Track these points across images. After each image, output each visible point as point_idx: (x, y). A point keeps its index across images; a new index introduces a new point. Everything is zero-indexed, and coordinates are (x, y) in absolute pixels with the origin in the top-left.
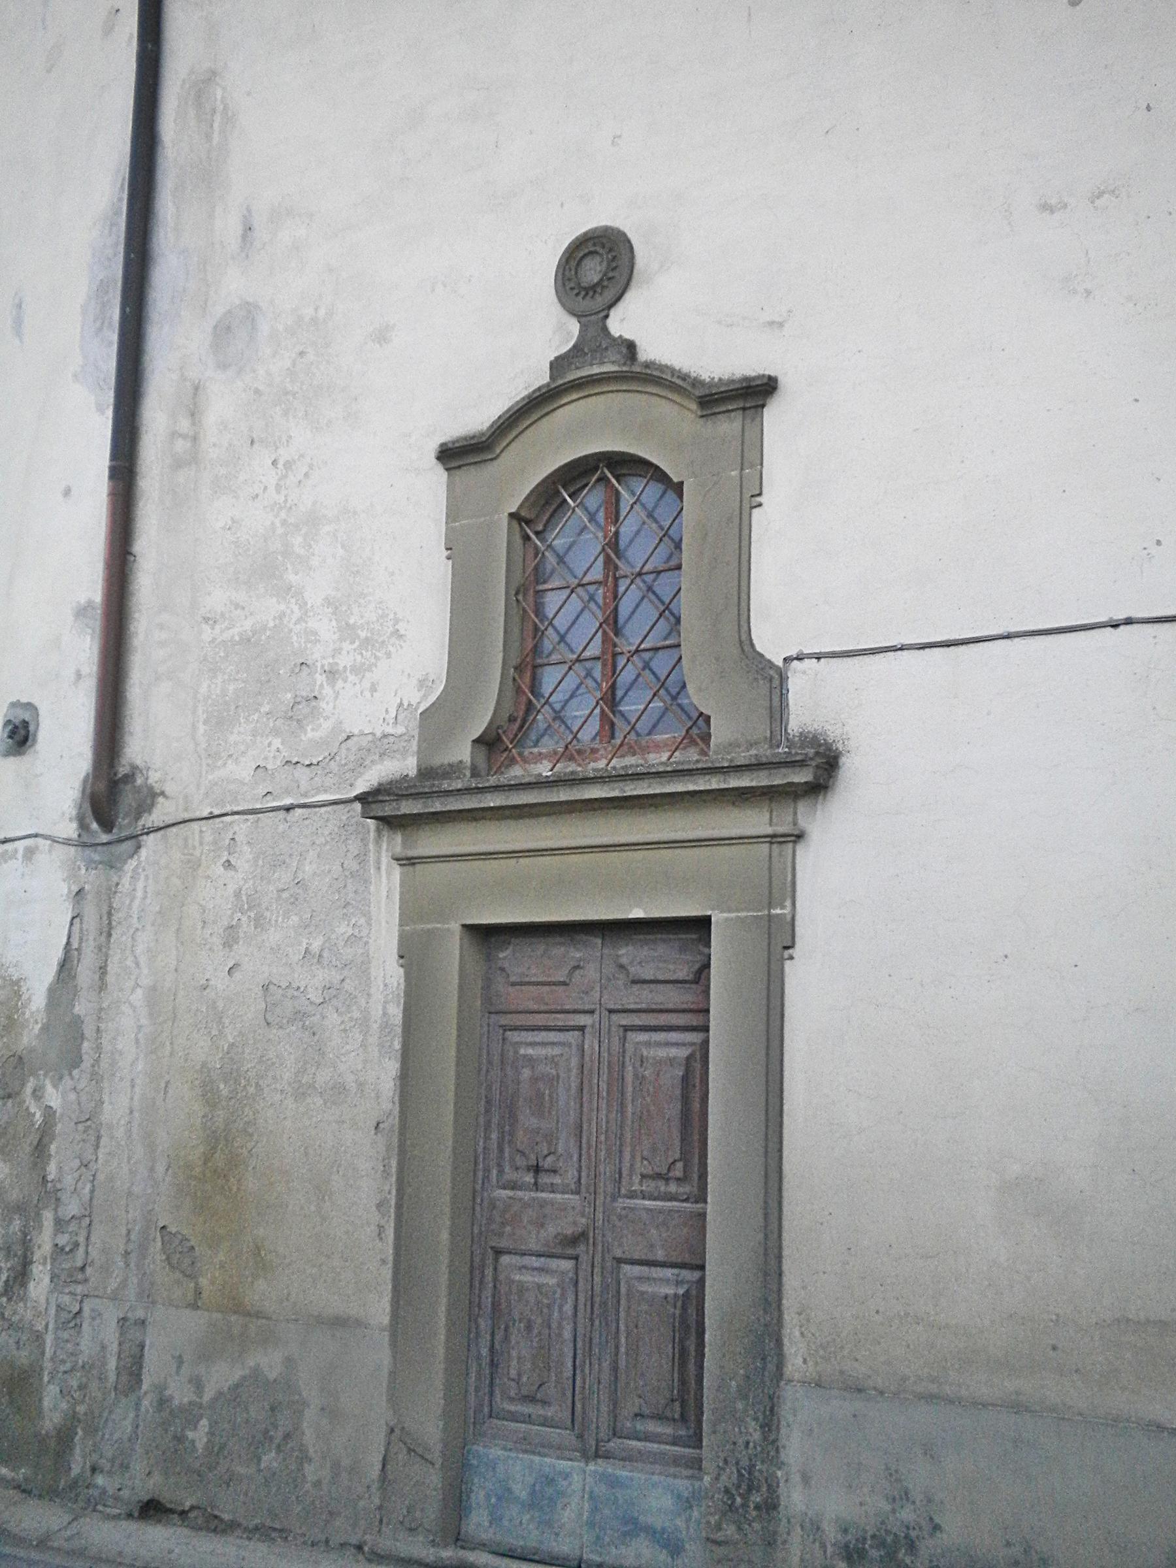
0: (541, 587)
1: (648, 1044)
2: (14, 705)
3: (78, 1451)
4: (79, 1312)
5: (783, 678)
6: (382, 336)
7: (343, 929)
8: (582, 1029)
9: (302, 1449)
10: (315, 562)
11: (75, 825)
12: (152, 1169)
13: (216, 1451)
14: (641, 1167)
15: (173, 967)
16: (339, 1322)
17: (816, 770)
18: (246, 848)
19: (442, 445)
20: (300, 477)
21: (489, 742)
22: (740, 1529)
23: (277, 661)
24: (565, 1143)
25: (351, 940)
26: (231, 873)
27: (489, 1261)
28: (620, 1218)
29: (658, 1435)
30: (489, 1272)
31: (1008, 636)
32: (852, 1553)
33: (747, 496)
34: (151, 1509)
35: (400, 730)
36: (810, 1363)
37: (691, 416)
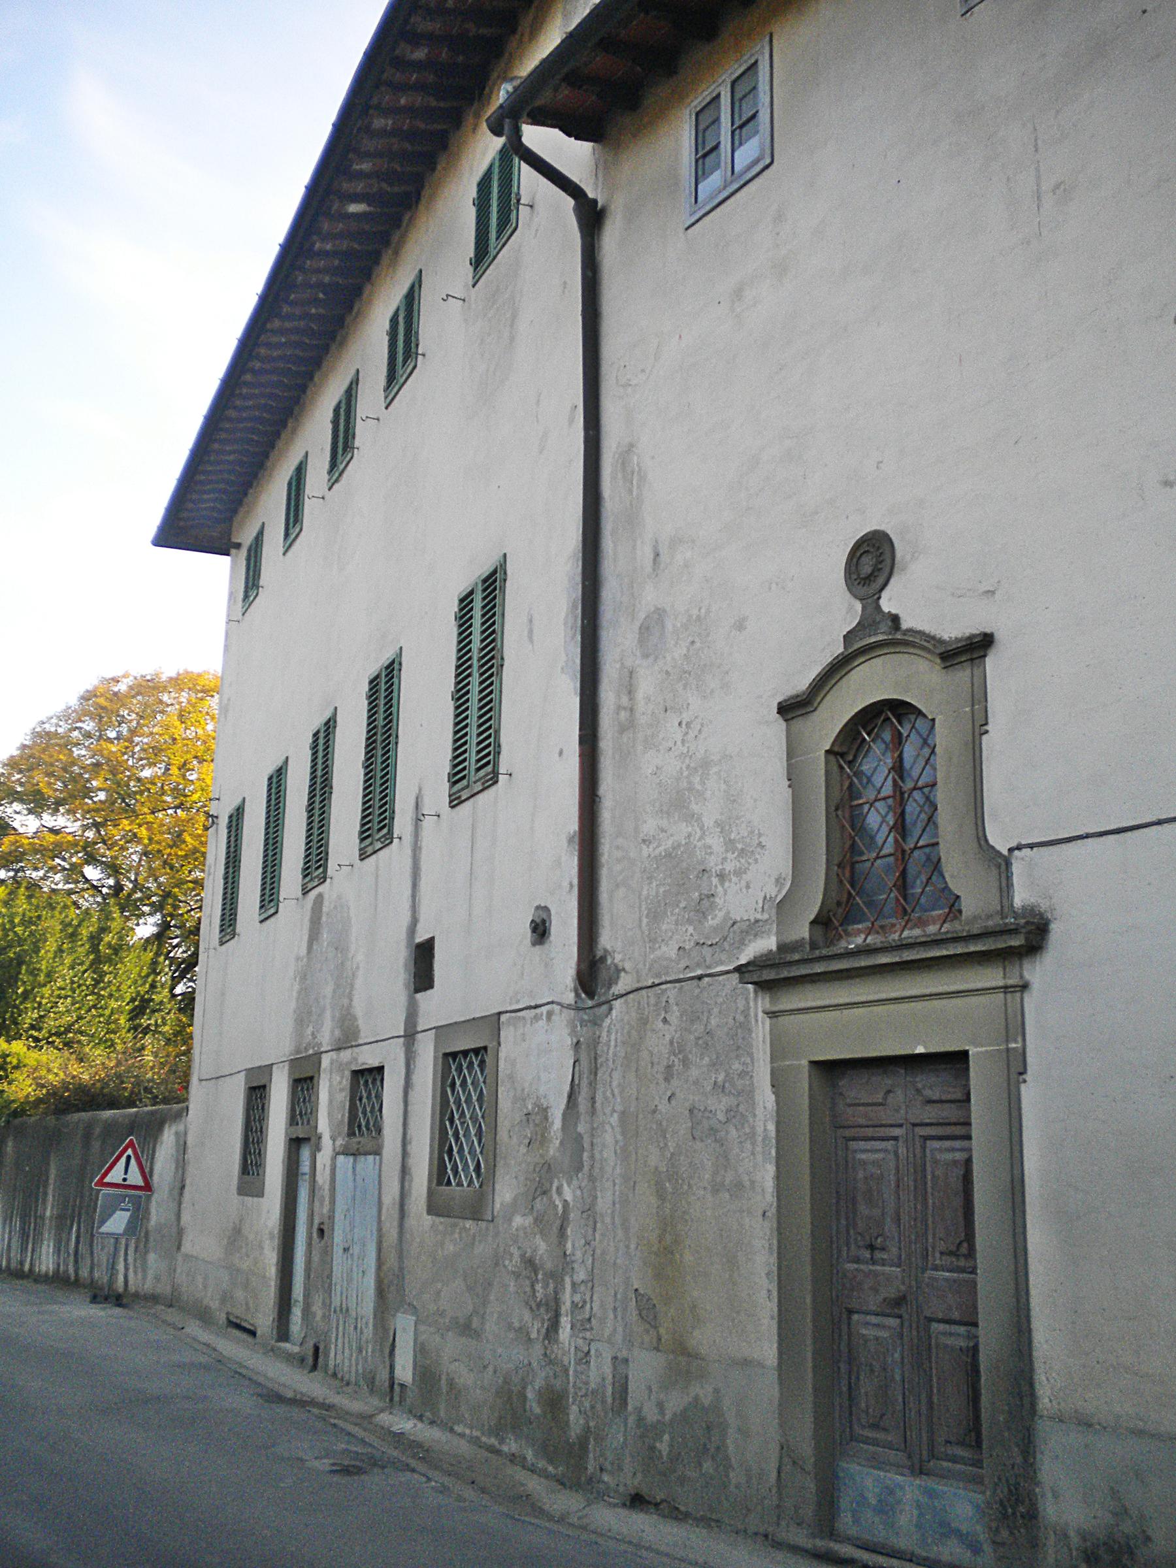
0: (855, 803)
1: (940, 1150)
2: (538, 908)
3: (591, 1455)
4: (589, 1352)
5: (1008, 863)
6: (740, 626)
7: (736, 1066)
8: (896, 1139)
9: (727, 1458)
10: (708, 794)
11: (573, 995)
12: (628, 1247)
13: (675, 1458)
14: (942, 1246)
15: (634, 1097)
16: (746, 1363)
17: (1029, 936)
18: (675, 1008)
19: (779, 703)
20: (696, 733)
21: (822, 922)
22: (1012, 1533)
23: (688, 869)
24: (889, 1226)
25: (743, 1074)
26: (667, 1027)
27: (844, 1316)
28: (928, 1285)
29: (963, 1458)
30: (844, 1327)
31: (1159, 823)
32: (1090, 1557)
33: (977, 725)
34: (637, 1501)
35: (766, 916)
36: (1054, 1403)
37: (937, 667)
